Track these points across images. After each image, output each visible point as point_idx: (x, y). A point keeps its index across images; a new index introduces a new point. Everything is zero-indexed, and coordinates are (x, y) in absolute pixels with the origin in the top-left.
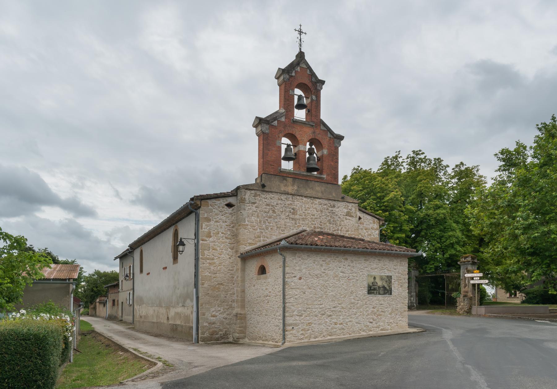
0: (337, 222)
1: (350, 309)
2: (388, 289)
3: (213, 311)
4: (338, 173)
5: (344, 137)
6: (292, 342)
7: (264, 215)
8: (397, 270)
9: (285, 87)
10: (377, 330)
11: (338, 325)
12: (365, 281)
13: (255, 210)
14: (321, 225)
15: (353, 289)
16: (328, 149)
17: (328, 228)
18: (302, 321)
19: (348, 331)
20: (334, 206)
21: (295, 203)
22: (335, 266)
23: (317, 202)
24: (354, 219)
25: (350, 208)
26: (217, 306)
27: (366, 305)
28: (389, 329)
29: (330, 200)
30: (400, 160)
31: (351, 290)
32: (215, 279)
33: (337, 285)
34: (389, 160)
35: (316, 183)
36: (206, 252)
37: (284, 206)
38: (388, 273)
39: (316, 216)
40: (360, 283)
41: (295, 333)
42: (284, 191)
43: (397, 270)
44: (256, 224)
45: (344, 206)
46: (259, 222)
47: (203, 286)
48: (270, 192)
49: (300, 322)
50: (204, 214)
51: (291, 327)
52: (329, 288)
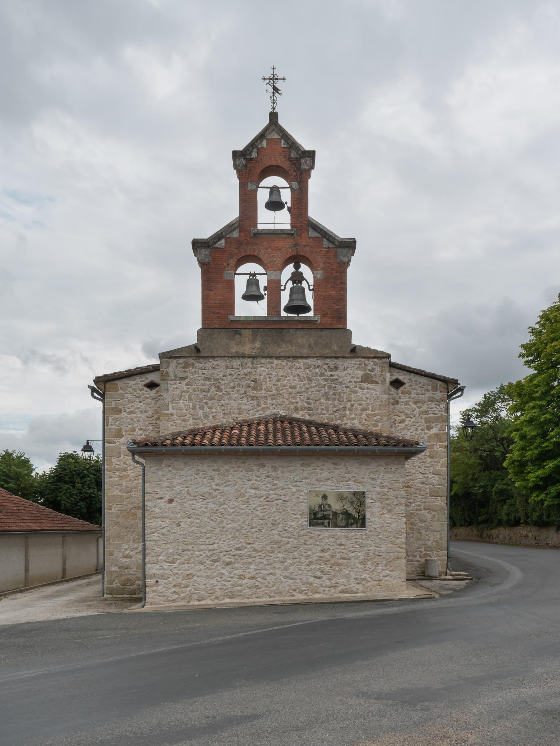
0: (342, 395)
1: (272, 552)
2: (356, 516)
3: (126, 550)
6: (156, 604)
7: (200, 396)
8: (379, 482)
10: (333, 590)
11: (247, 580)
12: (304, 503)
13: (185, 389)
14: (309, 404)
15: (276, 518)
16: (323, 269)
17: (324, 407)
18: (175, 571)
19: (267, 592)
20: (336, 368)
22: (239, 478)
24: (378, 387)
25: (370, 368)
26: (132, 541)
27: (306, 546)
28: (359, 591)
31: (272, 518)
32: (128, 500)
33: (243, 511)
36: (114, 460)
37: (236, 378)
38: (355, 487)
39: (298, 389)
40: (292, 507)
41: (161, 590)
43: (379, 482)
44: (187, 412)
47: (110, 511)
48: (211, 357)
49: (170, 573)
50: (111, 402)
51: (153, 581)
52: (226, 516)
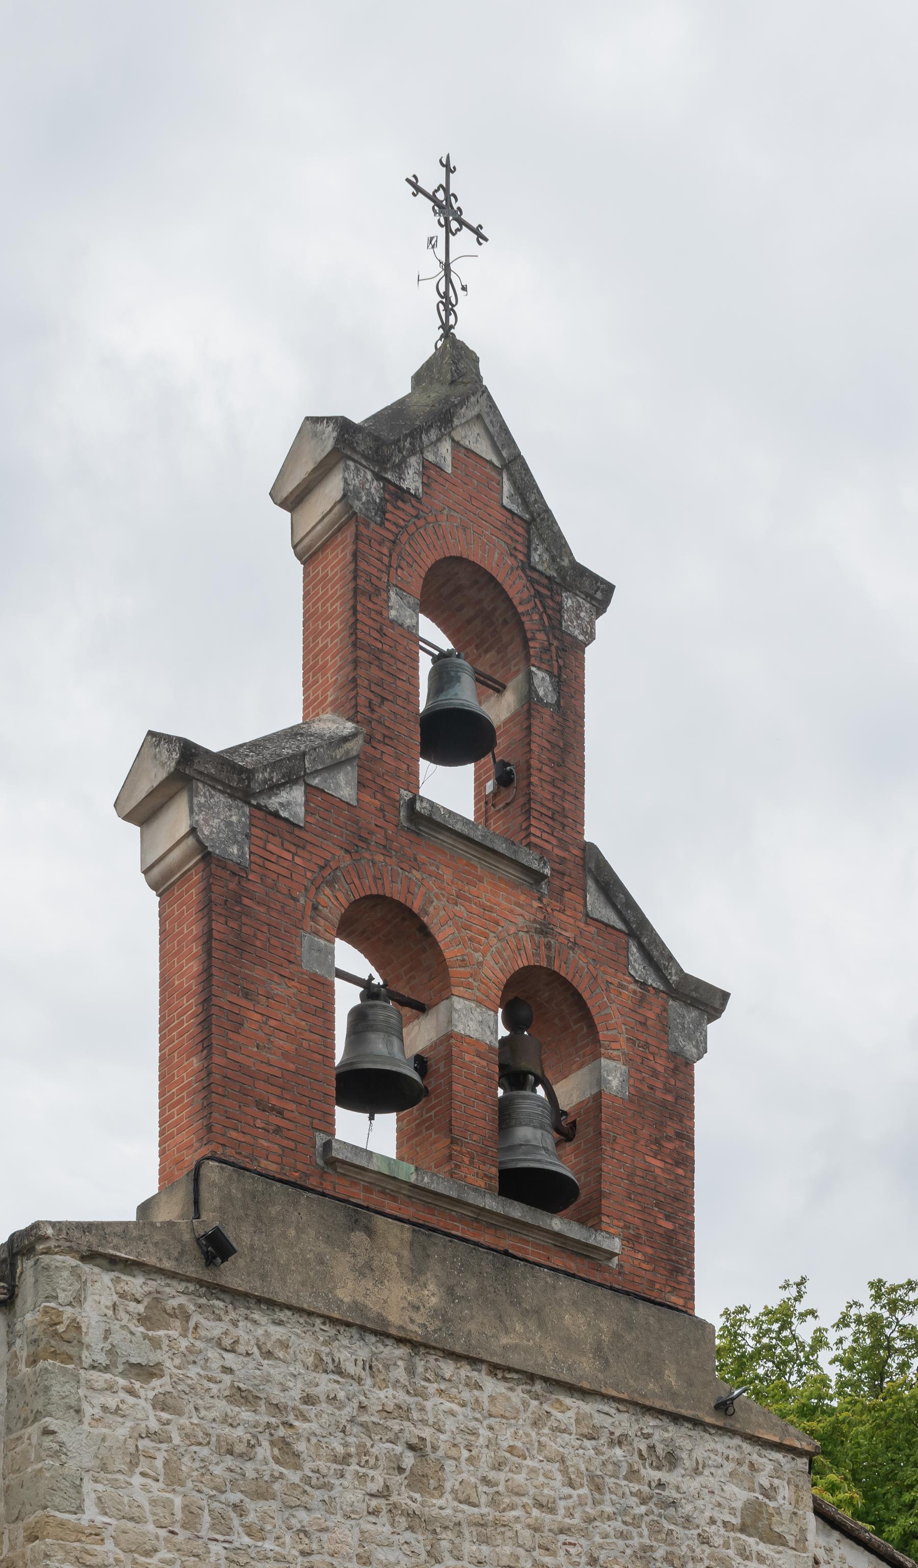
4: (691, 1237)
5: (725, 996)
7: (217, 1470)
9: (355, 555)
13: (154, 1425)
16: (628, 1061)
20: (672, 1460)
21: (429, 1405)
23: (567, 1418)
25: (766, 1484)
29: (648, 1410)
30: (804, 1331)
34: (745, 1328)
35: (562, 1282)
37: (352, 1421)
42: (356, 1306)
44: (163, 1533)
45: (729, 1467)
46: (179, 1515)
48: (260, 1300)
